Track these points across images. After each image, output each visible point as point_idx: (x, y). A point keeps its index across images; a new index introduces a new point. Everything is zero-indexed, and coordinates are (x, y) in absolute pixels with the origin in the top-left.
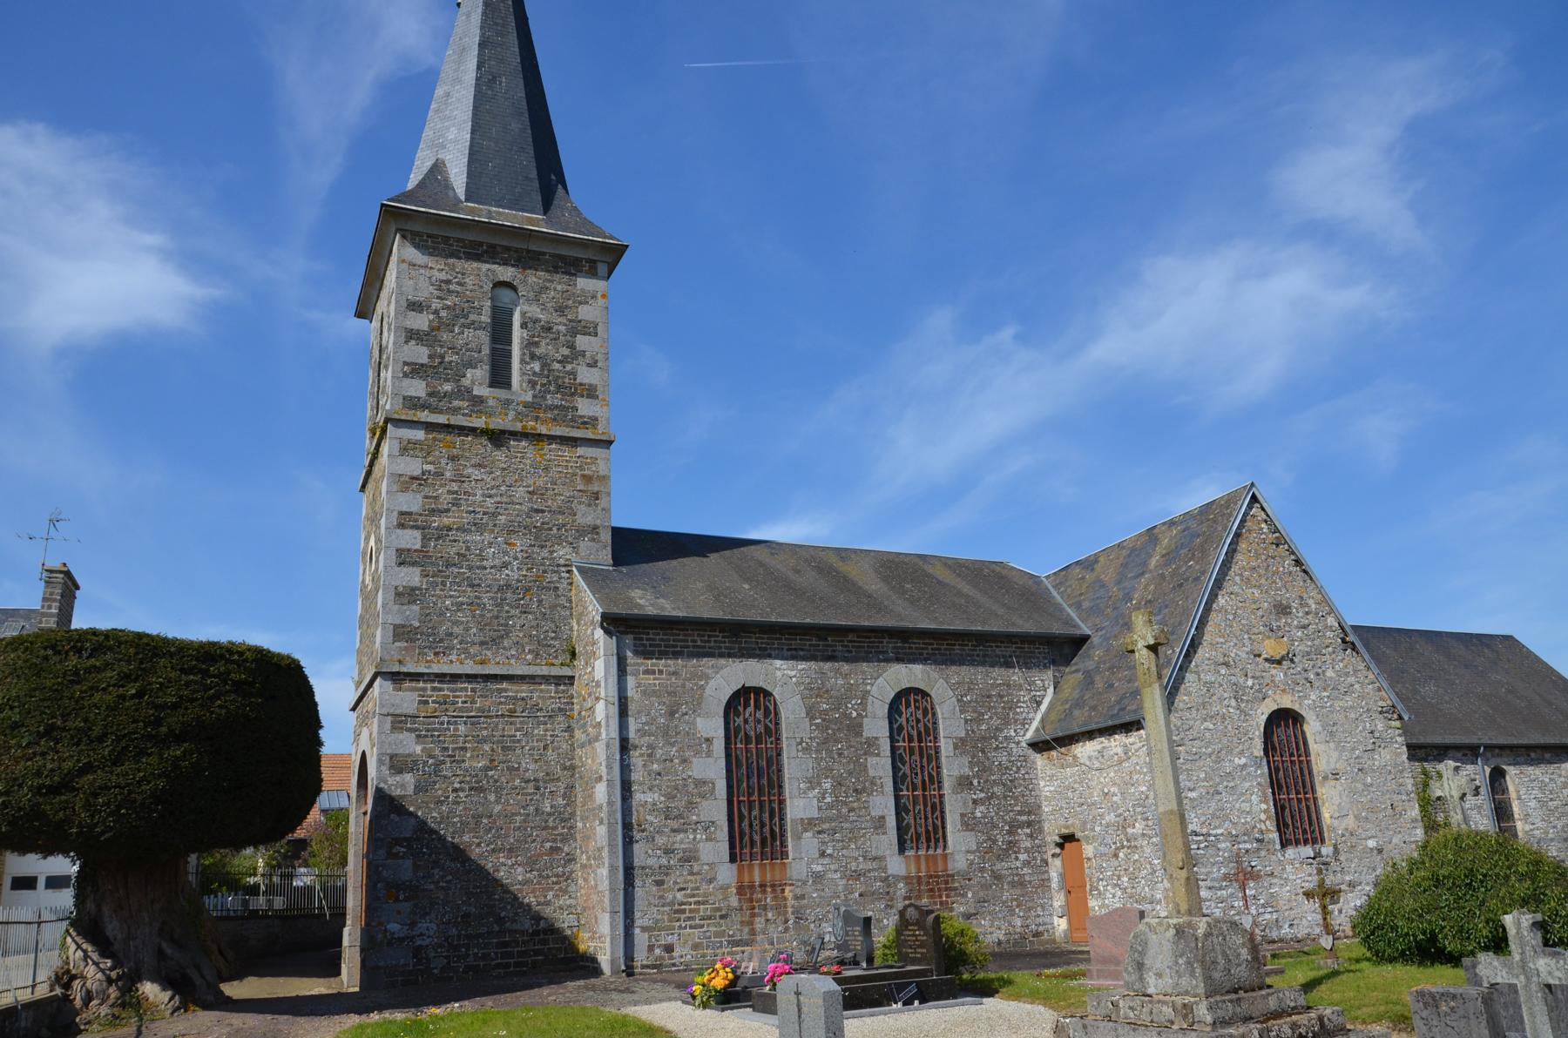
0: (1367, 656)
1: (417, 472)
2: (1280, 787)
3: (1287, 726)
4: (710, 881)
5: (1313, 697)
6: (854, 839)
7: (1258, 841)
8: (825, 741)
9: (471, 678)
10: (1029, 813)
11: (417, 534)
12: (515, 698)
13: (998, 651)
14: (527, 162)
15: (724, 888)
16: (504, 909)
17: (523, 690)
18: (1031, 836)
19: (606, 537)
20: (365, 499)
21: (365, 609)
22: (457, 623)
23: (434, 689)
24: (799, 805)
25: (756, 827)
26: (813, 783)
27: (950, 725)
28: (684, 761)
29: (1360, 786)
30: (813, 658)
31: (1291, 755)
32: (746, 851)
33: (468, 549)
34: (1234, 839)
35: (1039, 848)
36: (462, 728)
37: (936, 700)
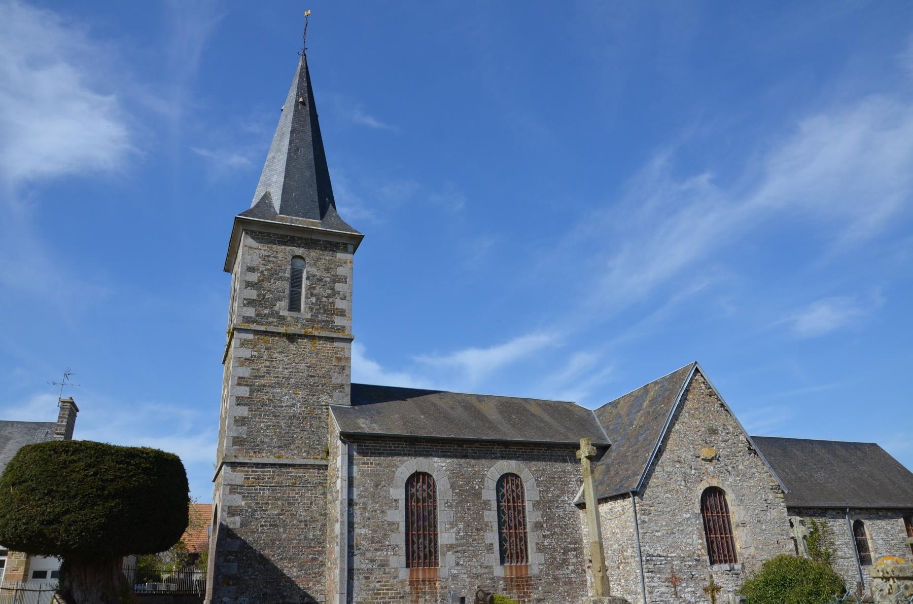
0: (763, 458)
1: (249, 356)
2: (710, 531)
3: (715, 496)
4: (395, 578)
6: (475, 556)
7: (696, 560)
8: (461, 502)
9: (273, 465)
10: (575, 543)
11: (247, 389)
12: (296, 476)
13: (559, 453)
14: (313, 192)
15: (402, 582)
16: (285, 591)
17: (300, 472)
18: (576, 556)
19: (348, 390)
20: (225, 367)
21: (222, 428)
22: (266, 436)
23: (253, 471)
24: (445, 537)
25: (421, 548)
26: (453, 525)
27: (531, 493)
28: (383, 512)
29: (758, 530)
30: (455, 457)
31: (718, 512)
32: (415, 561)
33: (274, 396)
34: (683, 560)
35: (581, 563)
36: (267, 492)
37: (523, 480)
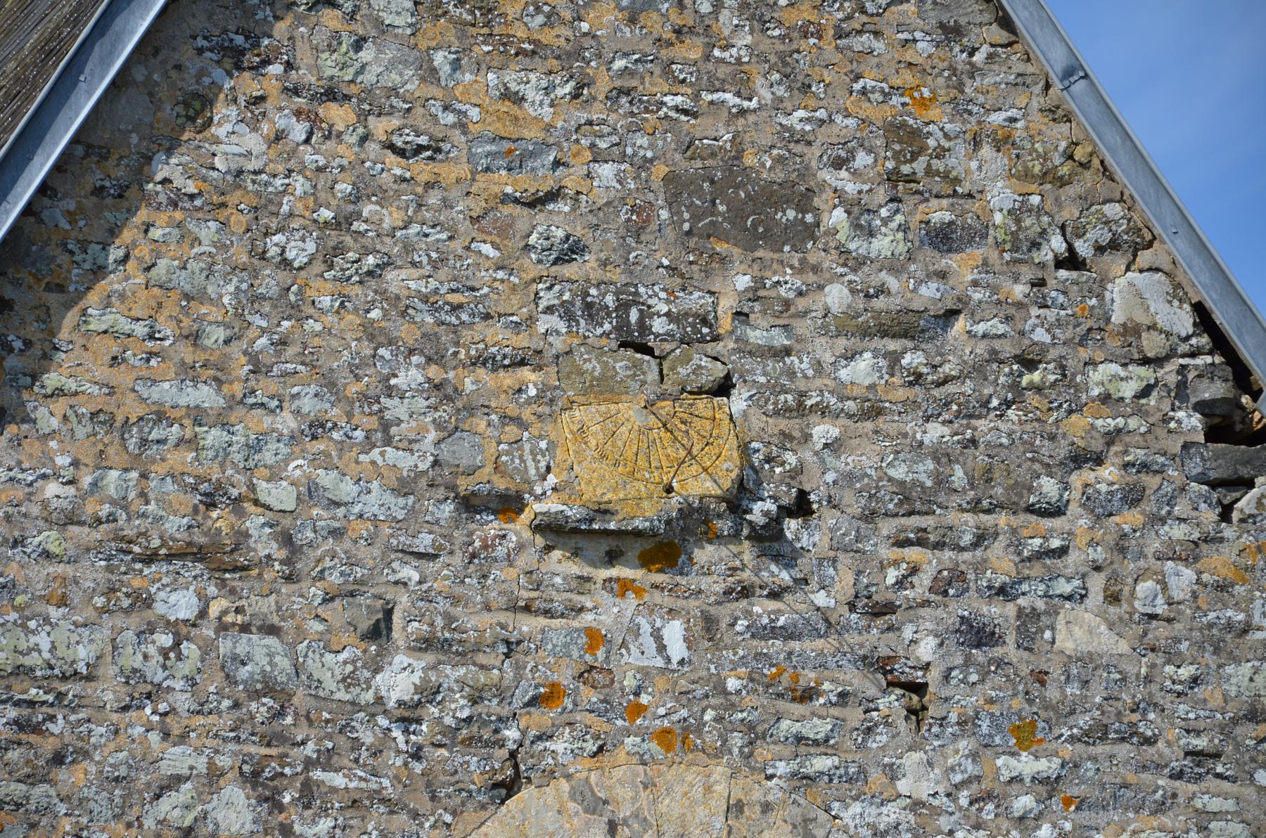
5: (918, 781)
